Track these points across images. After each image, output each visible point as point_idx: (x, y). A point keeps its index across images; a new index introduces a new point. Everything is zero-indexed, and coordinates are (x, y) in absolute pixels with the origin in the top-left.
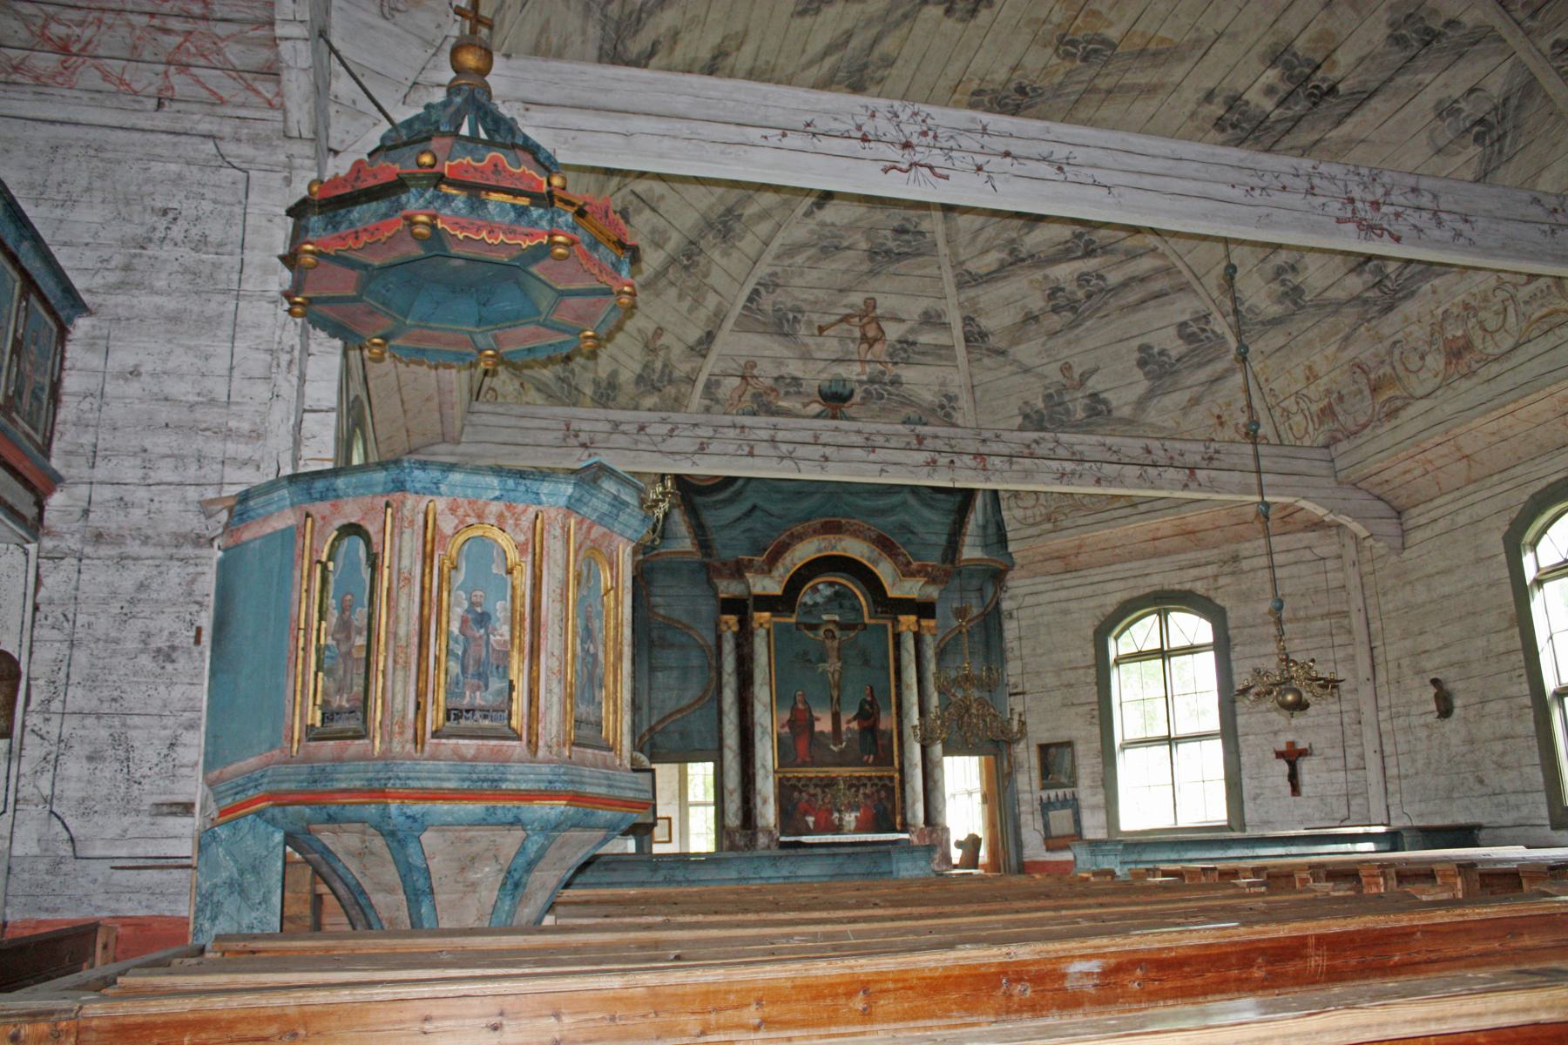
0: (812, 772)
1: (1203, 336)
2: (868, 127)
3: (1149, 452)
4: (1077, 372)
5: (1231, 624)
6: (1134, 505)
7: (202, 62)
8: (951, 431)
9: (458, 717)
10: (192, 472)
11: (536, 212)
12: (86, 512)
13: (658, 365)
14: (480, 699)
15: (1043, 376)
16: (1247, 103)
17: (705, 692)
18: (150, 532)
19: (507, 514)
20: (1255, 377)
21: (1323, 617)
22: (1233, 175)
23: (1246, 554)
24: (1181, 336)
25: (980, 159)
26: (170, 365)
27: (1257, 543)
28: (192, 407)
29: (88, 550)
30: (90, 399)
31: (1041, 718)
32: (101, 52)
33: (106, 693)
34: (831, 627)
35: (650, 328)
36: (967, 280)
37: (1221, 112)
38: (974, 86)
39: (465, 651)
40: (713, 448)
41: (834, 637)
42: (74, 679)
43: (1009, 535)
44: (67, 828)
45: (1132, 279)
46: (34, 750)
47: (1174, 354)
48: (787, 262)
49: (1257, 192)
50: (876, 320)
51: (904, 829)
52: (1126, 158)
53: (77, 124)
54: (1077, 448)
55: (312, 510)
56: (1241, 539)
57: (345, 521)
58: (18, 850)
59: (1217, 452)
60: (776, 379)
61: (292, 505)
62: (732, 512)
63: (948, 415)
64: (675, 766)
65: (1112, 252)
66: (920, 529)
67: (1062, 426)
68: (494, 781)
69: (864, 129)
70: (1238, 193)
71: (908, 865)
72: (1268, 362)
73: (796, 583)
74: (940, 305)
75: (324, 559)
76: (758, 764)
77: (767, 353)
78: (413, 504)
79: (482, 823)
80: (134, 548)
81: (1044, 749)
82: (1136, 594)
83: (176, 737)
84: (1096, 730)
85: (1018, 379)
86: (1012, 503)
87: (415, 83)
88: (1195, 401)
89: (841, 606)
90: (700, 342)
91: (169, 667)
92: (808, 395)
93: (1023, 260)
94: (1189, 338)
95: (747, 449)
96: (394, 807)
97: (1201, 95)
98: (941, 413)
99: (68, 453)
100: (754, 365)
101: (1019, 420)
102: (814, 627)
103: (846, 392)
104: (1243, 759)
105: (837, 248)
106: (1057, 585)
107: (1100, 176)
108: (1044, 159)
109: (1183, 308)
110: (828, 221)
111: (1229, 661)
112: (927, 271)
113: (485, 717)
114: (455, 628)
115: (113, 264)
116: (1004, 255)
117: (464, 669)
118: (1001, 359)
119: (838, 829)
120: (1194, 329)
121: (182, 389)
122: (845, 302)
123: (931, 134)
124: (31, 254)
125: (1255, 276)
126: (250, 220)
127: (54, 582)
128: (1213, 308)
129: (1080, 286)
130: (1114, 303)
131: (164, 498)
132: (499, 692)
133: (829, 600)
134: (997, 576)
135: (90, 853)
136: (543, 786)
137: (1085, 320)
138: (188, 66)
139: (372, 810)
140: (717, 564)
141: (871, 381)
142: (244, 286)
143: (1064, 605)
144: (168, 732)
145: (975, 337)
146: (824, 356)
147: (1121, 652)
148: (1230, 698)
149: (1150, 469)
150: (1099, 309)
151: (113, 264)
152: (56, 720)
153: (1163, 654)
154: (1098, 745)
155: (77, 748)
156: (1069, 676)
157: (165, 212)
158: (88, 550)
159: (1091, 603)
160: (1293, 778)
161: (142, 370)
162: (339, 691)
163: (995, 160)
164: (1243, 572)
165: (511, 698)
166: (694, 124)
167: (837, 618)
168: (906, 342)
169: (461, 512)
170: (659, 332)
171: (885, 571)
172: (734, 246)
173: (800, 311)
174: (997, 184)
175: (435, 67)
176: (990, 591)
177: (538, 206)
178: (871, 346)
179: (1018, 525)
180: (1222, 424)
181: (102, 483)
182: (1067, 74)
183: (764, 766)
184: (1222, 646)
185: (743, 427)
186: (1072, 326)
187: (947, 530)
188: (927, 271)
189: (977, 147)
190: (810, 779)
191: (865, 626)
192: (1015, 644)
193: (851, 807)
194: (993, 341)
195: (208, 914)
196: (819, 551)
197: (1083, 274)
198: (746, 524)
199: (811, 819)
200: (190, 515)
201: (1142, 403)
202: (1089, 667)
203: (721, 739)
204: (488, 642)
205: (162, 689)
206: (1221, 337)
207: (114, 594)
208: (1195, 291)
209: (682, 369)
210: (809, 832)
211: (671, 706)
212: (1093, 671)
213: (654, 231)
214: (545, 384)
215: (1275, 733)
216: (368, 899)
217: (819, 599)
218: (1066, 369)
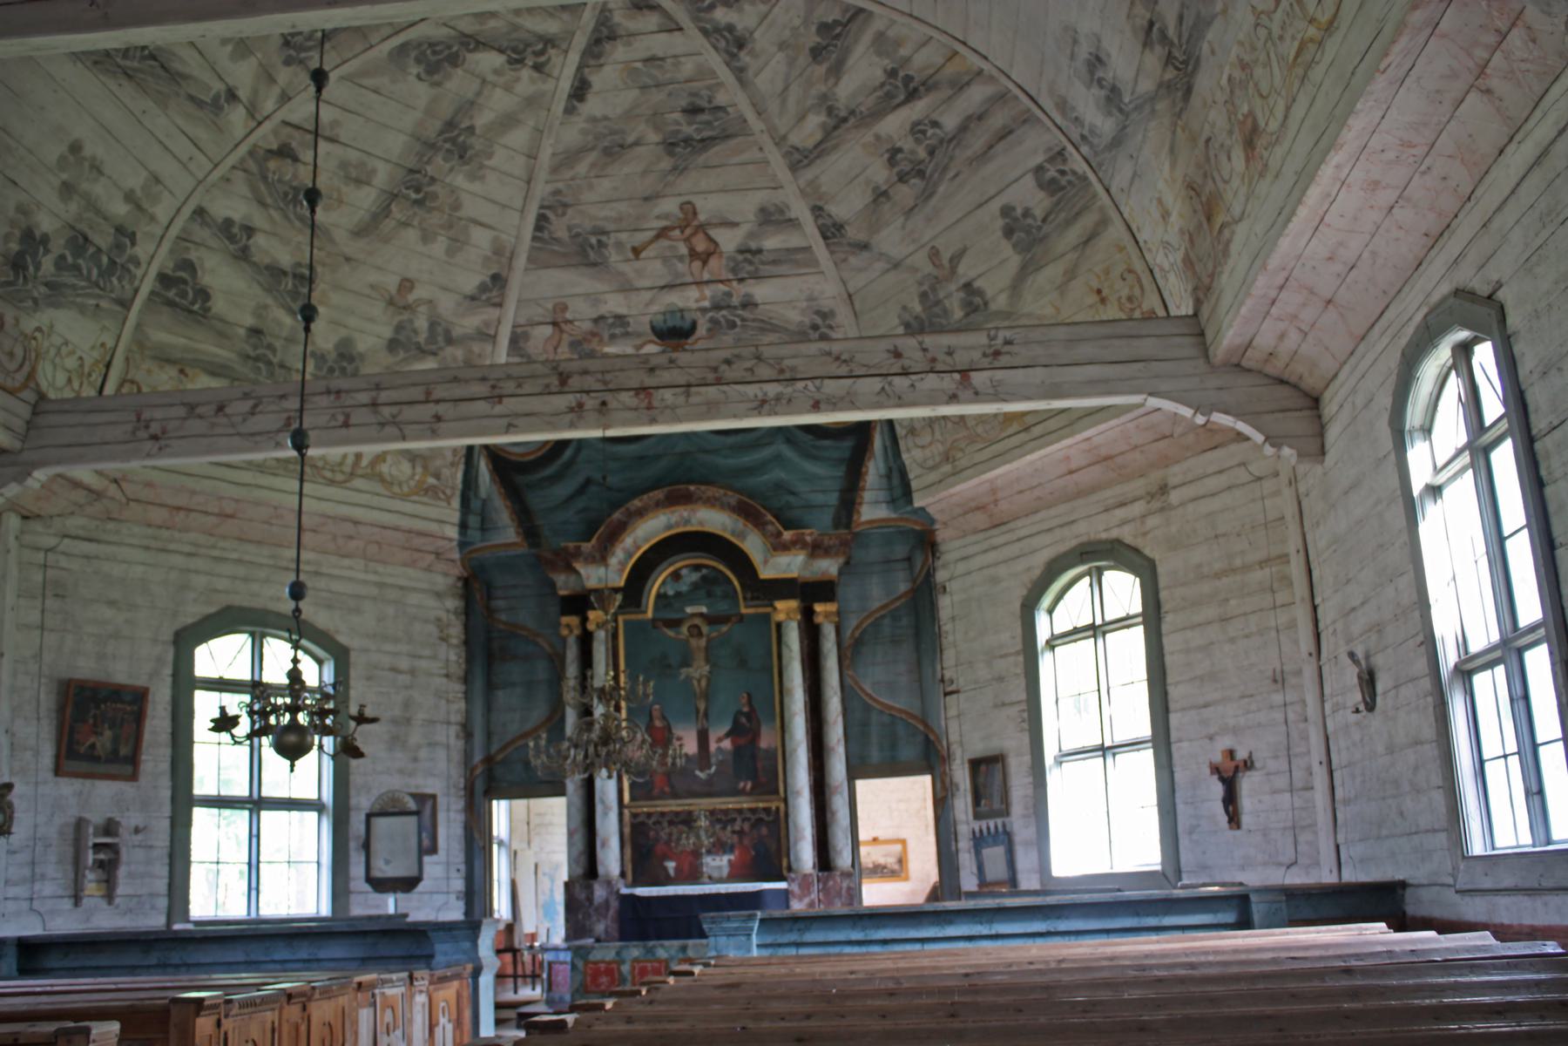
0: (672, 806)
1: (1063, 181)
3: (897, 354)
4: (946, 257)
5: (1163, 581)
13: (422, 323)
15: (915, 270)
21: (1262, 564)
31: (968, 731)
34: (697, 621)
35: (392, 283)
41: (700, 634)
43: (914, 485)
45: (969, 118)
47: (1039, 213)
48: (568, 174)
50: (702, 228)
54: (787, 363)
56: (1166, 461)
59: (1008, 342)
62: (561, 490)
64: (1560, 735)
66: (802, 487)
67: (941, 330)
81: (976, 765)
88: (1071, 274)
89: (709, 594)
90: (483, 288)
92: (639, 335)
93: (845, 120)
94: (1051, 187)
95: (341, 418)
100: (565, 308)
101: (901, 330)
102: (675, 624)
103: (687, 325)
104: (1177, 776)
105: (622, 146)
106: (985, 545)
109: (1032, 147)
110: (598, 113)
111: (1159, 635)
112: (745, 157)
118: (865, 255)
120: (1052, 173)
122: (657, 211)
129: (918, 141)
133: (695, 586)
141: (717, 307)
145: (832, 232)
146: (647, 283)
149: (897, 380)
153: (1095, 631)
159: (1020, 566)
160: (1231, 799)
167: (704, 610)
168: (749, 251)
170: (407, 284)
171: (753, 545)
172: (482, 166)
178: (705, 263)
184: (1152, 616)
185: (338, 392)
186: (926, 195)
188: (745, 157)
190: (663, 814)
191: (741, 618)
193: (719, 847)
196: (669, 527)
197: (916, 124)
198: (581, 503)
211: (514, 729)
212: (1021, 658)
215: (1211, 738)
217: (684, 588)
218: (934, 254)
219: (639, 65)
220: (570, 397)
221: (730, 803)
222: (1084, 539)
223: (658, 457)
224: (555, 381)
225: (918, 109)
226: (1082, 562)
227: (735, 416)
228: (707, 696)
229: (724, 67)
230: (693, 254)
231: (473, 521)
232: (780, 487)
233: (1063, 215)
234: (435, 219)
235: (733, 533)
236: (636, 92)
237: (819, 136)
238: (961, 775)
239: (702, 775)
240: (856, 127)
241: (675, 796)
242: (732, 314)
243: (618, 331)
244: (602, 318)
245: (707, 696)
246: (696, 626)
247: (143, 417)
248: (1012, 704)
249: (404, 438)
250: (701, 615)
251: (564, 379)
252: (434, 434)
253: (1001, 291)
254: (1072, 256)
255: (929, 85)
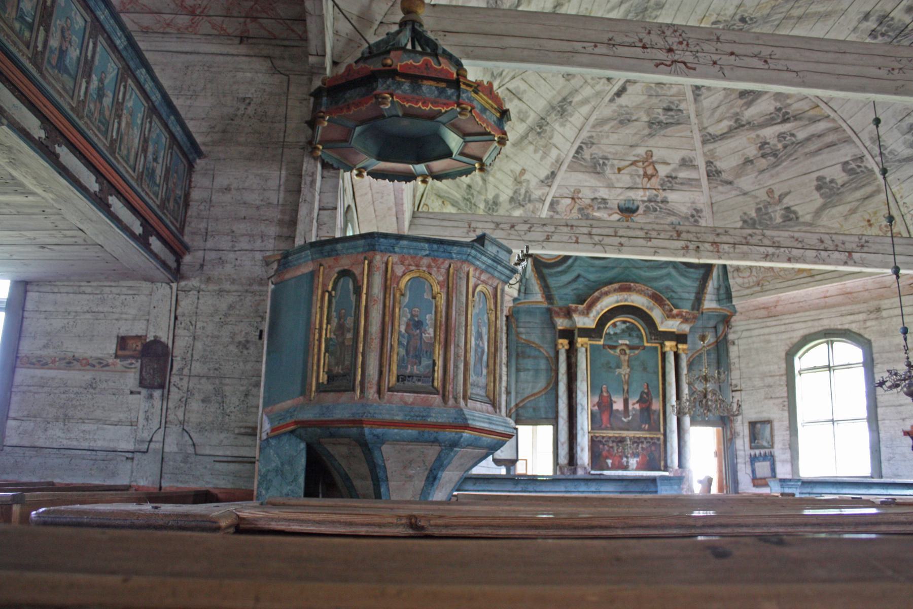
0: (611, 433)
1: (859, 170)
2: (646, 40)
3: (822, 241)
5: (875, 350)
6: (812, 276)
7: (264, 15)
8: (698, 229)
9: (403, 380)
10: (258, 244)
11: (450, 91)
12: (202, 266)
13: (523, 191)
14: (416, 370)
16: (892, 19)
17: (548, 385)
18: (235, 277)
19: (433, 264)
20: (894, 196)
22: (879, 61)
23: (885, 307)
24: (844, 170)
25: (715, 57)
26: (247, 184)
27: (893, 300)
28: (258, 208)
29: (203, 286)
30: (204, 204)
32: (211, 13)
33: (212, 366)
34: (624, 347)
35: (518, 169)
36: (709, 139)
37: (875, 26)
38: (713, 19)
39: (408, 343)
40: (554, 238)
41: (625, 354)
42: (196, 357)
43: (733, 294)
44: (191, 438)
45: (813, 136)
46: (175, 395)
47: (840, 182)
49: (896, 71)
50: (653, 163)
51: (666, 468)
52: (808, 53)
53: (198, 53)
54: (776, 239)
55: (323, 262)
56: (881, 297)
57: (341, 268)
58: (167, 449)
59: (867, 242)
60: (593, 200)
61: (312, 260)
63: (696, 221)
65: (800, 119)
66: (679, 290)
67: (767, 227)
68: (423, 417)
69: (644, 41)
70: (883, 73)
71: (667, 487)
72: (903, 186)
73: (603, 321)
74: (692, 154)
75: (330, 288)
76: (579, 428)
77: (587, 184)
78: (378, 259)
79: (416, 440)
80: (227, 286)
81: (753, 424)
82: (812, 330)
83: (248, 391)
84: (786, 414)
85: (740, 199)
86: (735, 274)
87: (381, 23)
89: (630, 335)
90: (547, 178)
91: (245, 352)
92: (611, 209)
93: (743, 126)
94: (851, 172)
95: (574, 239)
96: (367, 430)
97: (862, 15)
98: (692, 220)
99: (193, 233)
100: (579, 192)
101: (740, 224)
102: (614, 348)
103: (634, 207)
104: (881, 435)
105: (629, 121)
107: (792, 65)
108: (756, 56)
109: (846, 153)
110: (624, 104)
113: (419, 380)
114: (403, 329)
115: (216, 129)
116: (732, 123)
117: (407, 353)
118: (729, 187)
119: (626, 468)
120: (853, 165)
121: (252, 198)
122: (634, 153)
123: (685, 43)
124: (175, 123)
125: (896, 131)
126: (290, 103)
127: (186, 304)
128: (866, 152)
129: (779, 141)
130: (802, 151)
131: (244, 258)
132: (427, 366)
133: (623, 331)
134: (726, 320)
135: (203, 452)
136: (451, 421)
137: (782, 162)
138: (257, 18)
139: (354, 431)
140: (557, 309)
141: (650, 201)
142: (286, 140)
143: (767, 337)
144: (245, 388)
145: (713, 174)
146: (621, 185)
147: (803, 368)
148: (873, 386)
149: (822, 252)
150: (791, 155)
151: (216, 129)
152: (186, 379)
154: (786, 423)
155: (196, 395)
156: (770, 380)
157: (244, 99)
158: (203, 286)
159: (784, 336)
161: (232, 187)
162: (337, 364)
163: (724, 57)
164: (883, 318)
165: (434, 371)
166: (541, 41)
167: (627, 342)
168: (671, 177)
169: (407, 262)
170: (523, 171)
171: (657, 314)
172: (567, 120)
173: (607, 159)
174: (726, 72)
175: (392, 14)
176: (721, 328)
177: (451, 88)
178: (649, 179)
179: (739, 288)
180: (870, 225)
181: (210, 250)
182: (773, 8)
183: (582, 429)
184: (869, 364)
185: (572, 226)
186: (774, 165)
187: (694, 290)
189: (713, 50)
190: (610, 437)
191: (644, 348)
192: (736, 360)
193: (635, 455)
194: (724, 176)
195: (264, 486)
196: (617, 302)
198: (575, 286)
199: (609, 462)
200: (257, 268)
201: (818, 213)
202: (782, 375)
203: (557, 412)
204: (421, 338)
205: (241, 364)
206: (871, 171)
207: (217, 311)
208: (854, 142)
209: (537, 193)
210: (608, 469)
211: (529, 391)
212: (784, 378)
213: (520, 112)
214: (457, 202)
215: (903, 420)
216: (351, 483)
217: (618, 331)
218: (770, 192)
219: (653, 85)
220: (683, 242)
221: (639, 434)
222: (827, 327)
223: (613, 268)
224: (675, 235)
225: (786, 127)
226: (825, 337)
227: (755, 260)
228: (628, 383)
229: (691, 93)
230: (645, 175)
231: (523, 290)
232: (668, 288)
233: (854, 185)
234: (542, 142)
235: (647, 307)
236: (645, 97)
237: (725, 130)
238: (741, 428)
239: (625, 420)
240: (747, 130)
241: (612, 429)
242: (656, 205)
243: (602, 206)
244: (596, 198)
245: (628, 383)
246: (624, 350)
247: (472, 226)
248: (778, 398)
249: (606, 252)
250: (626, 345)
251: (679, 234)
252: (620, 251)
253: (808, 213)
254: (857, 203)
255: (796, 118)
